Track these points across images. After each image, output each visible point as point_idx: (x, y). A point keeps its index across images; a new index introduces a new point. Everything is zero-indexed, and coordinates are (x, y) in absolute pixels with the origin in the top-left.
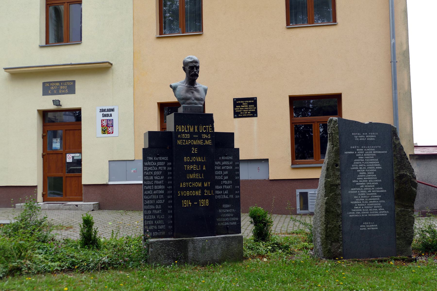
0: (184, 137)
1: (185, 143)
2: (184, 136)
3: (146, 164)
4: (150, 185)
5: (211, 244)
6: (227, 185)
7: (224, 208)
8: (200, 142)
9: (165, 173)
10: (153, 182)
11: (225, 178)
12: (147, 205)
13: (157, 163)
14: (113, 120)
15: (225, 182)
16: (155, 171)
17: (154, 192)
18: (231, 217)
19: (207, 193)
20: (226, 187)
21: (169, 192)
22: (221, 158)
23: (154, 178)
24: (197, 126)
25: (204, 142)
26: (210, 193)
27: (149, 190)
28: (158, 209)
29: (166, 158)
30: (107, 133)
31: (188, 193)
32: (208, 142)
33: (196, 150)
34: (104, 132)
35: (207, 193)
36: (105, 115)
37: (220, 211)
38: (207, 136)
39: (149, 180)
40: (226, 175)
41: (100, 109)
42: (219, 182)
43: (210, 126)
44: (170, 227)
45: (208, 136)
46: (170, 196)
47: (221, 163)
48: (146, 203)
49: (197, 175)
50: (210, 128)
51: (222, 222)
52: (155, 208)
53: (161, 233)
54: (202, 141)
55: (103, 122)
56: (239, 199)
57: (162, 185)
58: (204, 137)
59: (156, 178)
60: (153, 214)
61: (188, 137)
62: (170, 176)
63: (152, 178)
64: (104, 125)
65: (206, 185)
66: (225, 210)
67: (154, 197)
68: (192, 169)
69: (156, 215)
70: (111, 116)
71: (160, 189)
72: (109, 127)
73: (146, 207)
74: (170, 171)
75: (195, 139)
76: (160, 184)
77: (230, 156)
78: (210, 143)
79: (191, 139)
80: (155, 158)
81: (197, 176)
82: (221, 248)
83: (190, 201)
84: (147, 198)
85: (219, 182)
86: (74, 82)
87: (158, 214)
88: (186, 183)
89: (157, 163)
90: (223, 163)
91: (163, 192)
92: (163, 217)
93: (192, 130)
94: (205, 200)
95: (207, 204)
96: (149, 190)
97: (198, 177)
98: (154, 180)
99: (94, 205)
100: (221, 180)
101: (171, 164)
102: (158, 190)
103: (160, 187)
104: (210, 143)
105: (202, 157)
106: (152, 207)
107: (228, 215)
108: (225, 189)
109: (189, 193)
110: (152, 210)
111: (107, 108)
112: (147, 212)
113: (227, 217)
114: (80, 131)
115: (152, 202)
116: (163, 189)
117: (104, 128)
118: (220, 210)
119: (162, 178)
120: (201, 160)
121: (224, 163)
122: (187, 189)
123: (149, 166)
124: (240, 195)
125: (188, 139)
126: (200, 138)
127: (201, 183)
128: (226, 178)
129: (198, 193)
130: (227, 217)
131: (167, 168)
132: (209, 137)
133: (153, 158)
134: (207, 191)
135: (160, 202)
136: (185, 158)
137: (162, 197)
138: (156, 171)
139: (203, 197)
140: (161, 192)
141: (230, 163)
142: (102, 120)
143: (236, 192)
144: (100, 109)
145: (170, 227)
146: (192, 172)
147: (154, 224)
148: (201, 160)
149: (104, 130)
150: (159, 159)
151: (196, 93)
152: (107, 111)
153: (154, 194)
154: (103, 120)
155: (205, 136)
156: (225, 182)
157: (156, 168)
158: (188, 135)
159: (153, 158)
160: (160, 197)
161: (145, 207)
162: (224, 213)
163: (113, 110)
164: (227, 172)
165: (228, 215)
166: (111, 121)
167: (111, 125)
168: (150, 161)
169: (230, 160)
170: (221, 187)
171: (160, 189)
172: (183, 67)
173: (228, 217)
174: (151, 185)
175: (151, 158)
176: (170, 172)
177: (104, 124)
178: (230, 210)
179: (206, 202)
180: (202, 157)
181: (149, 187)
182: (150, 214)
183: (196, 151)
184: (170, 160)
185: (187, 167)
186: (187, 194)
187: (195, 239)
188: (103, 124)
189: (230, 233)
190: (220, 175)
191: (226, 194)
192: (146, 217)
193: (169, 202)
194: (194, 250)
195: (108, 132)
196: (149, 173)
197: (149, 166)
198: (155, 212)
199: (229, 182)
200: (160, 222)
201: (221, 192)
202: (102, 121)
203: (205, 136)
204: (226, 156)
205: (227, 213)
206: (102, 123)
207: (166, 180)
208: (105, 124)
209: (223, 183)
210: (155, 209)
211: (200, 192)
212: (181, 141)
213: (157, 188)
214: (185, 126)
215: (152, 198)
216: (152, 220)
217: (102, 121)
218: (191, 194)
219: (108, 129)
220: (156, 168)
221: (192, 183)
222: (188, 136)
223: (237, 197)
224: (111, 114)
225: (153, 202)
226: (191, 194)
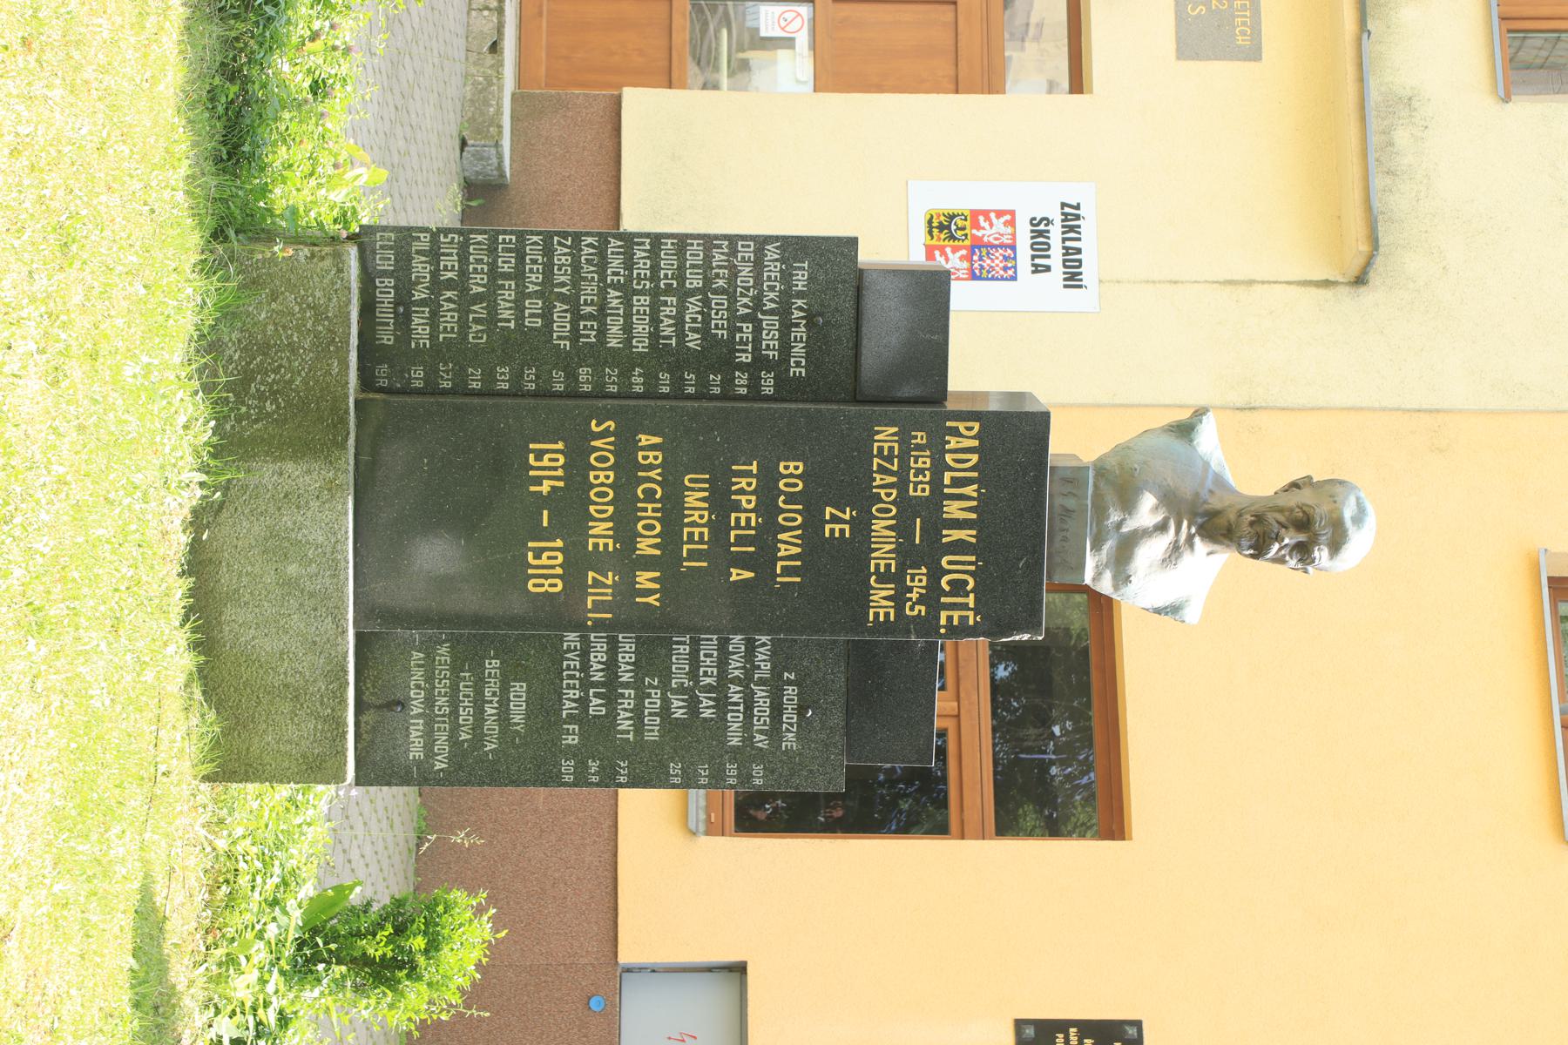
0: (916, 462)
1: (882, 470)
2: (920, 465)
3: (771, 253)
4: (655, 268)
5: (312, 595)
6: (638, 715)
7: (505, 688)
8: (883, 555)
9: (718, 355)
10: (669, 290)
11: (676, 704)
12: (548, 251)
13: (772, 312)
14: (1014, 278)
15: (653, 703)
16: (732, 299)
17: (613, 293)
18: (455, 729)
19: (601, 588)
20: (628, 703)
21: (611, 374)
22: (790, 683)
23: (692, 293)
24: (973, 540)
25: (884, 578)
26: (598, 607)
27: (629, 264)
28: (519, 308)
29: (798, 364)
30: (934, 242)
31: (602, 477)
32: (880, 601)
33: (842, 531)
34: (941, 227)
35: (597, 584)
36: (1041, 234)
37: (492, 666)
38: (914, 596)
39: (681, 268)
40: (693, 706)
41: (1078, 207)
42: (652, 660)
43: (971, 614)
44: (418, 375)
45: (919, 602)
46: (587, 382)
47: (762, 682)
48: (560, 243)
49: (701, 534)
50: (961, 617)
51: (430, 678)
52: (530, 296)
53: (387, 324)
54: (888, 566)
55: (999, 224)
56: (550, 778)
57: (655, 336)
58: (912, 580)
59: (693, 306)
60: (495, 279)
61: (915, 490)
62: (703, 383)
63: (695, 282)
64: (979, 228)
65: (645, 579)
66: (494, 694)
67: (589, 291)
68: (737, 507)
69: (490, 297)
70: (1037, 269)
71: (628, 328)
72: (969, 258)
73: (535, 243)
74: (728, 382)
75: (902, 528)
76: (657, 328)
77: (798, 737)
78: (877, 615)
79: (903, 502)
80: (800, 302)
81: (697, 530)
82: (282, 653)
83: (561, 484)
84: (587, 250)
85: (652, 660)
86: (1254, 53)
87: (493, 309)
88: (657, 467)
89: (772, 312)
90: (760, 693)
91: (613, 343)
92: (477, 335)
93: (953, 510)
94: (559, 571)
95: (535, 585)
96: (629, 264)
97: (691, 534)
98: (684, 294)
99: (493, 151)
100: (666, 677)
101: (768, 390)
102: (628, 316)
103: (641, 328)
104: (877, 615)
105: (799, 563)
106: (534, 279)
107: (466, 714)
108: (611, 699)
109: (602, 484)
110: (519, 275)
111: (1088, 243)
112: (510, 250)
113: (454, 705)
114: (952, 87)
115: (563, 279)
116: (628, 341)
117: (963, 229)
118: (496, 663)
119: (693, 341)
120: (782, 559)
121: (761, 695)
122: (627, 468)
123: (758, 265)
124: (575, 784)
125: (902, 485)
126: (908, 556)
127: (658, 552)
128: (679, 711)
129: (600, 533)
130: (454, 705)
131: (742, 367)
132: (912, 609)
133: (800, 295)
134: (606, 586)
135: (562, 323)
136: (796, 468)
137: (588, 336)
138: (732, 309)
139: (578, 563)
140: (615, 329)
141: (761, 732)
142: (1012, 213)
143: (594, 766)
144: (1078, 207)
145: (418, 375)
146: (721, 502)
147: (437, 285)
148: (782, 559)
149: (949, 227)
150: (797, 325)
151: (1160, 544)
152: (1068, 244)
153: (602, 293)
154: (1012, 223)
155: (918, 582)
156: (653, 703)
157: (746, 306)
158: (923, 490)
159: (800, 295)
160: (585, 326)
161: (535, 238)
162: (479, 692)
163: (1073, 278)
164: (707, 714)
165: (466, 714)
166: (1005, 269)
167: (982, 267)
168: (786, 277)
169: (775, 732)
170: (626, 678)
171: (628, 328)
172: (1309, 477)
173: (454, 713)
174: (654, 277)
175: (801, 280)
176: (722, 385)
177: (986, 225)
178: (491, 726)
179: (546, 577)
180: (799, 563)
181: (643, 267)
182: (493, 266)
183: (832, 531)
184: (788, 389)
185: (748, 474)
186: (595, 469)
187: (345, 504)
188: (988, 219)
189: (364, 718)
190: (694, 674)
191: (583, 702)
192: (479, 243)
193: (557, 376)
194: (286, 496)
195: (936, 247)
196: (719, 267)
197: (758, 265)
198: (508, 294)
199: (653, 726)
200: (449, 318)
201: (598, 677)
202: (1008, 217)
203: (918, 582)
204: (801, 710)
205: (479, 703)
206: (993, 215)
207: (677, 360)
208: (988, 231)
209: (651, 686)
210: (522, 295)
211: (606, 545)
212: (891, 449)
213: (638, 311)
214: (975, 474)
215: (585, 279)
216: (463, 273)
217: (1008, 217)
218: (597, 494)
219: (954, 252)
220: (746, 306)
221: (656, 501)
222: (920, 489)
223: (567, 767)
224: (1048, 269)
225: (563, 285)
226: (597, 494)
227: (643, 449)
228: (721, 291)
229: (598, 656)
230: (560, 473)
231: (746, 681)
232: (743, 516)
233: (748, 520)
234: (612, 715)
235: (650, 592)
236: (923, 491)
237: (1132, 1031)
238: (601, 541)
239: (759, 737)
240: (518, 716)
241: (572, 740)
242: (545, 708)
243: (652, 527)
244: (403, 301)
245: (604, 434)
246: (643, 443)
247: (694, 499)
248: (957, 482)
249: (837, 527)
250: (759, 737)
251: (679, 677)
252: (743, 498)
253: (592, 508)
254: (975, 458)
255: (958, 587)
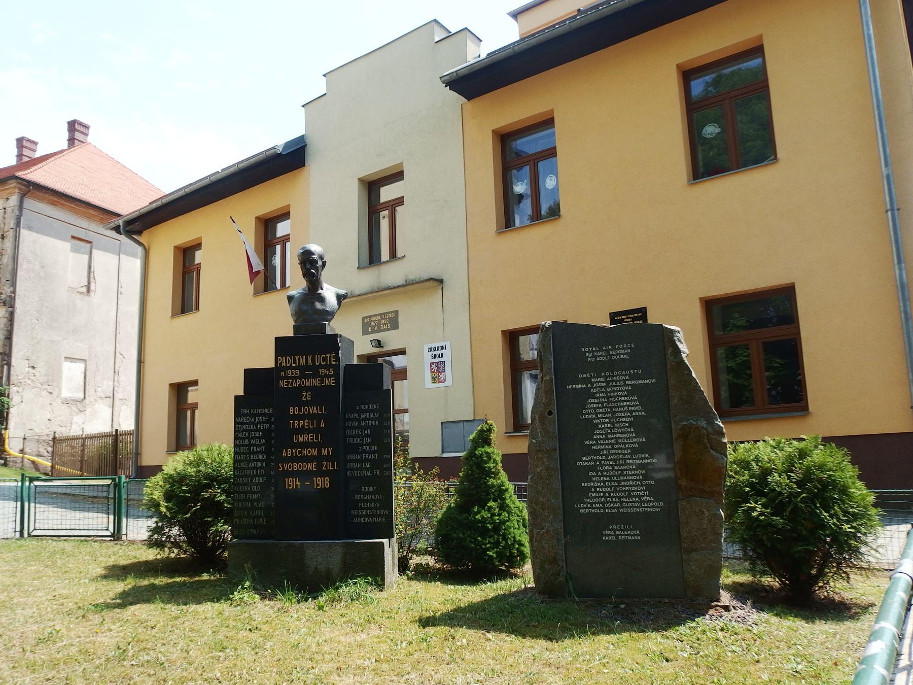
3: (239, 420)
6: (370, 453)
8: (316, 382)
10: (249, 449)
11: (367, 441)
15: (366, 448)
16: (252, 430)
23: (250, 442)
25: (322, 381)
29: (269, 411)
31: (295, 467)
33: (309, 395)
34: (435, 380)
38: (327, 372)
40: (367, 436)
45: (329, 371)
47: (359, 416)
51: (361, 516)
52: (251, 489)
55: (433, 366)
57: (262, 453)
65: (324, 452)
68: (303, 426)
70: (442, 356)
71: (259, 460)
75: (308, 377)
78: (333, 383)
79: (300, 377)
80: (252, 411)
85: (355, 449)
93: (303, 362)
97: (311, 439)
102: (256, 461)
103: (259, 456)
104: (333, 383)
107: (373, 505)
108: (366, 461)
118: (356, 496)
119: (263, 441)
122: (294, 459)
125: (296, 378)
126: (316, 375)
129: (311, 466)
133: (250, 411)
139: (320, 473)
146: (302, 431)
154: (433, 363)
155: (323, 371)
156: (366, 448)
159: (250, 411)
163: (444, 348)
164: (369, 432)
168: (245, 415)
170: (359, 457)
171: (259, 460)
173: (372, 508)
175: (246, 411)
178: (374, 497)
185: (294, 423)
190: (358, 436)
191: (367, 469)
199: (373, 448)
201: (359, 465)
203: (323, 371)
205: (368, 501)
209: (362, 449)
225: (248, 480)
227: (287, 455)
228: (249, 434)
229: (353, 465)
230: (294, 479)
231: (360, 421)
232: (306, 424)
233: (307, 422)
234: (370, 460)
235: (328, 450)
236: (297, 372)
237: (612, 315)
238: (314, 466)
239: (376, 416)
240: (371, 489)
241: (378, 472)
242: (367, 481)
243: (309, 451)
244: (255, 527)
245: (283, 466)
246: (285, 455)
247: (301, 439)
248: (295, 362)
249: (308, 396)
250: (376, 416)
251: (358, 440)
252: (301, 424)
253: (304, 469)
254: (288, 357)
255: (325, 359)
